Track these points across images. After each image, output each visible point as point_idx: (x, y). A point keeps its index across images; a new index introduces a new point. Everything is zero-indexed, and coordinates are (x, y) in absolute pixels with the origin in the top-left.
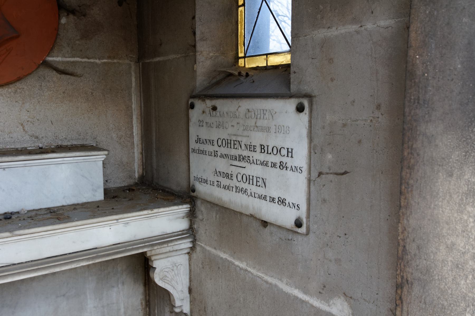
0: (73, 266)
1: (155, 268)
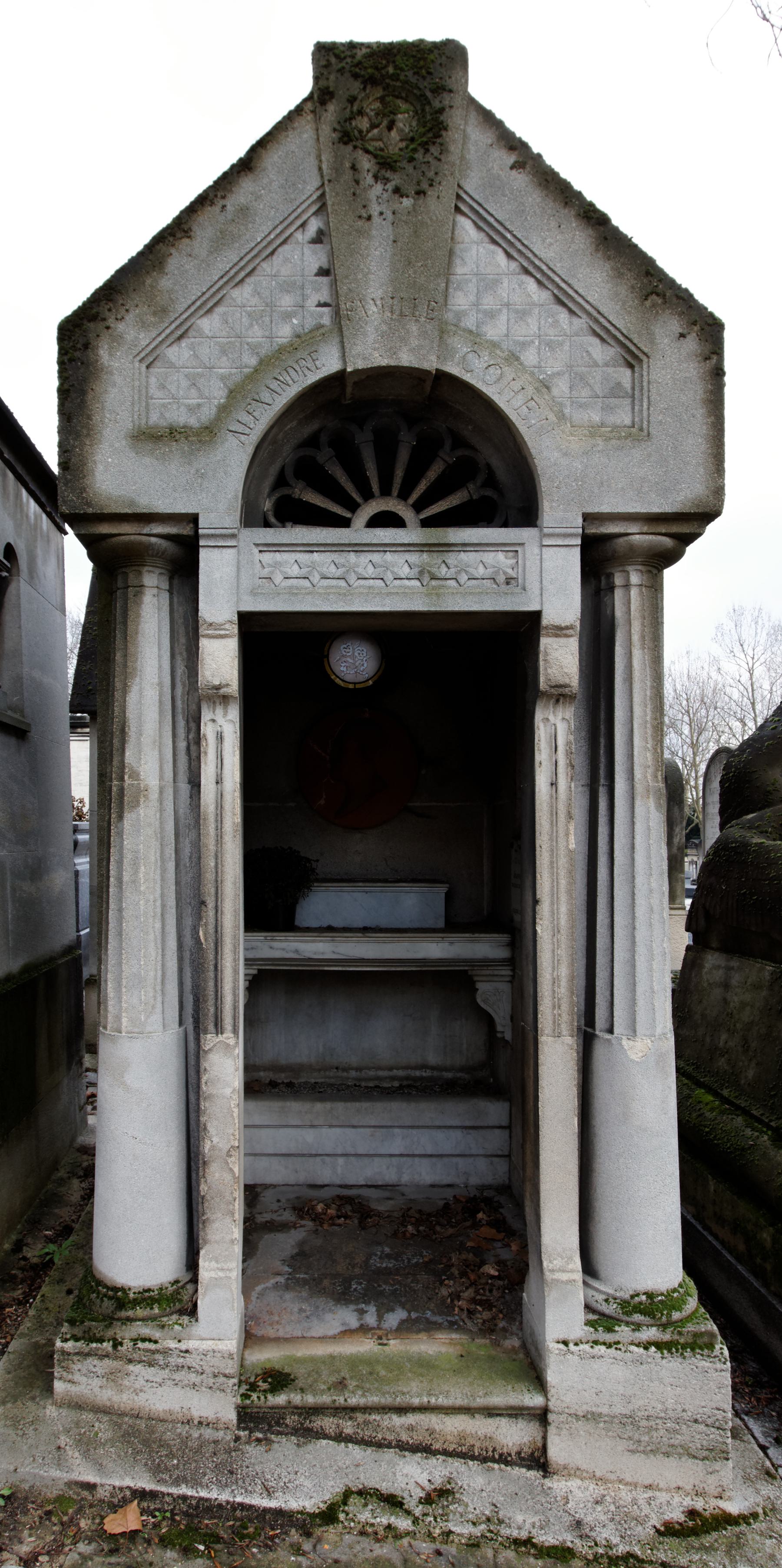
0: (405, 969)
1: (478, 989)
